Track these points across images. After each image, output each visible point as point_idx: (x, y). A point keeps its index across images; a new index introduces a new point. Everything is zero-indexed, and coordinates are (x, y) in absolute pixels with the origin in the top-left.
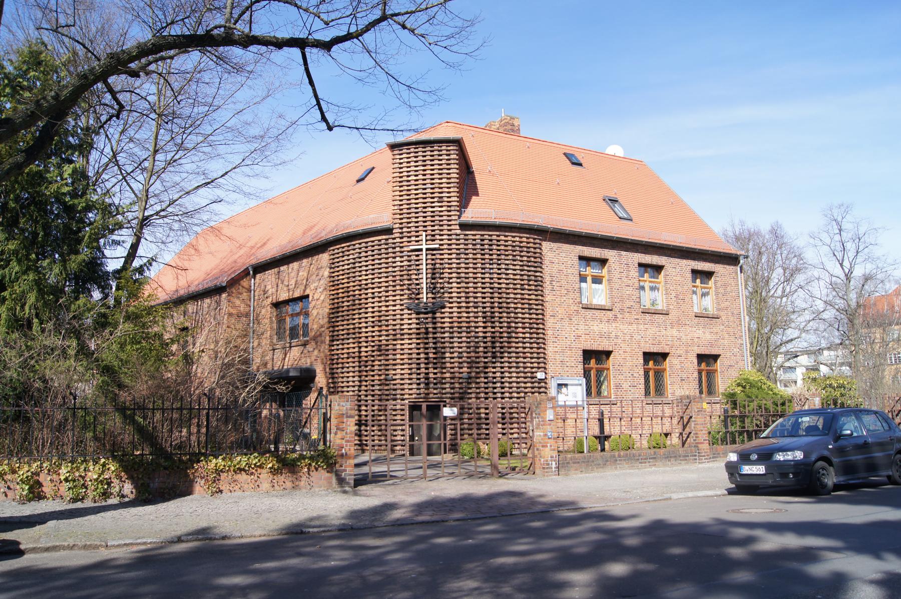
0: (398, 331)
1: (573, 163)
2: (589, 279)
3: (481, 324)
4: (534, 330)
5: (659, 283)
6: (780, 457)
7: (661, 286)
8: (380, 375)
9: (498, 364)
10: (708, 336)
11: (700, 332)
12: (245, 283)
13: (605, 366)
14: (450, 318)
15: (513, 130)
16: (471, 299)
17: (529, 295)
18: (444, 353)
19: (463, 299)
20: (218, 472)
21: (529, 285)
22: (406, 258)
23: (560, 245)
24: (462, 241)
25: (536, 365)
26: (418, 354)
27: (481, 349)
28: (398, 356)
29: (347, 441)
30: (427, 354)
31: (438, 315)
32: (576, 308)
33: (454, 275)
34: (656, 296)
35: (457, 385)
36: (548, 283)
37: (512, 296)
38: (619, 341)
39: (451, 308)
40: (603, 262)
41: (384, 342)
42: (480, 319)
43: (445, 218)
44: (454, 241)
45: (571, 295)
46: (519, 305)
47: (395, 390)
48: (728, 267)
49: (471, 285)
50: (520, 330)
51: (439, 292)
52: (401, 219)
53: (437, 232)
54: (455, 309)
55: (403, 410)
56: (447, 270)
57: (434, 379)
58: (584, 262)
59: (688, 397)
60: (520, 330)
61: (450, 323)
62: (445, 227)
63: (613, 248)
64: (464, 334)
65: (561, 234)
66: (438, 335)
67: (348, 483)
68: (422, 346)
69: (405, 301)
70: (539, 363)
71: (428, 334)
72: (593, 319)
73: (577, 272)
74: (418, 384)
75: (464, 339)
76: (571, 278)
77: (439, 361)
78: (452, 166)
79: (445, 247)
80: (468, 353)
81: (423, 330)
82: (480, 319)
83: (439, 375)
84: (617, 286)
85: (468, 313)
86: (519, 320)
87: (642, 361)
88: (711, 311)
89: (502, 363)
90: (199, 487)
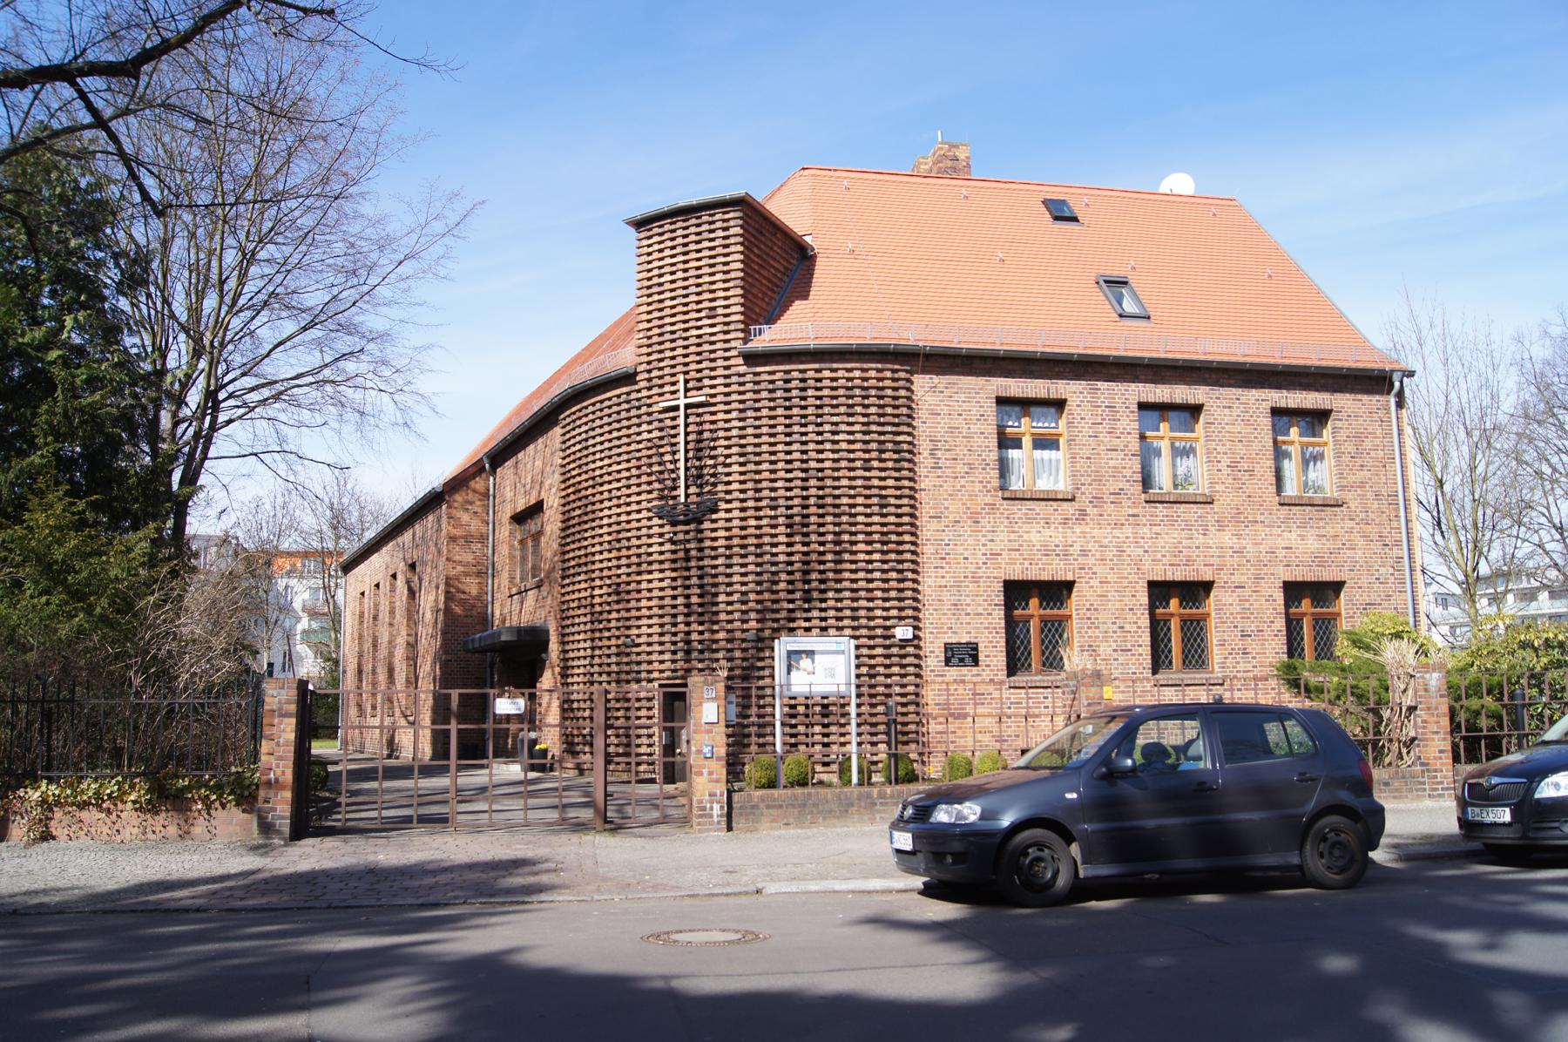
0: (644, 558)
1: (1057, 218)
2: (1027, 441)
3: (782, 539)
5: (1326, 444)
6: (942, 815)
7: (1199, 447)
9: (815, 613)
10: (1312, 544)
11: (1294, 536)
12: (478, 484)
13: (1062, 612)
14: (728, 529)
15: (954, 169)
16: (766, 493)
17: (881, 479)
18: (716, 595)
19: (750, 494)
20: (46, 805)
21: (882, 460)
22: (656, 424)
24: (749, 386)
25: (894, 613)
26: (674, 597)
27: (782, 585)
28: (644, 603)
29: (280, 758)
30: (688, 597)
31: (707, 525)
32: (988, 500)
33: (735, 450)
35: (737, 654)
36: (926, 454)
37: (845, 482)
38: (1091, 561)
39: (728, 511)
40: (1059, 405)
41: (624, 578)
42: (782, 529)
43: (719, 346)
44: (735, 388)
45: (979, 475)
46: (860, 500)
47: (639, 663)
48: (1365, 398)
49: (765, 466)
50: (862, 547)
51: (707, 483)
52: (649, 354)
53: (706, 373)
54: (736, 513)
55: (650, 699)
56: (723, 442)
57: (700, 642)
60: (862, 547)
62: (720, 363)
63: (1077, 376)
64: (751, 559)
67: (279, 832)
68: (679, 582)
69: (655, 503)
70: (901, 609)
72: (1029, 520)
73: (993, 430)
74: (674, 652)
75: (751, 568)
76: (978, 441)
77: (706, 611)
79: (720, 398)
80: (758, 593)
82: (782, 529)
83: (707, 635)
84: (1086, 452)
85: (758, 518)
87: (1145, 600)
88: (1330, 493)
89: (822, 610)
90: (19, 830)
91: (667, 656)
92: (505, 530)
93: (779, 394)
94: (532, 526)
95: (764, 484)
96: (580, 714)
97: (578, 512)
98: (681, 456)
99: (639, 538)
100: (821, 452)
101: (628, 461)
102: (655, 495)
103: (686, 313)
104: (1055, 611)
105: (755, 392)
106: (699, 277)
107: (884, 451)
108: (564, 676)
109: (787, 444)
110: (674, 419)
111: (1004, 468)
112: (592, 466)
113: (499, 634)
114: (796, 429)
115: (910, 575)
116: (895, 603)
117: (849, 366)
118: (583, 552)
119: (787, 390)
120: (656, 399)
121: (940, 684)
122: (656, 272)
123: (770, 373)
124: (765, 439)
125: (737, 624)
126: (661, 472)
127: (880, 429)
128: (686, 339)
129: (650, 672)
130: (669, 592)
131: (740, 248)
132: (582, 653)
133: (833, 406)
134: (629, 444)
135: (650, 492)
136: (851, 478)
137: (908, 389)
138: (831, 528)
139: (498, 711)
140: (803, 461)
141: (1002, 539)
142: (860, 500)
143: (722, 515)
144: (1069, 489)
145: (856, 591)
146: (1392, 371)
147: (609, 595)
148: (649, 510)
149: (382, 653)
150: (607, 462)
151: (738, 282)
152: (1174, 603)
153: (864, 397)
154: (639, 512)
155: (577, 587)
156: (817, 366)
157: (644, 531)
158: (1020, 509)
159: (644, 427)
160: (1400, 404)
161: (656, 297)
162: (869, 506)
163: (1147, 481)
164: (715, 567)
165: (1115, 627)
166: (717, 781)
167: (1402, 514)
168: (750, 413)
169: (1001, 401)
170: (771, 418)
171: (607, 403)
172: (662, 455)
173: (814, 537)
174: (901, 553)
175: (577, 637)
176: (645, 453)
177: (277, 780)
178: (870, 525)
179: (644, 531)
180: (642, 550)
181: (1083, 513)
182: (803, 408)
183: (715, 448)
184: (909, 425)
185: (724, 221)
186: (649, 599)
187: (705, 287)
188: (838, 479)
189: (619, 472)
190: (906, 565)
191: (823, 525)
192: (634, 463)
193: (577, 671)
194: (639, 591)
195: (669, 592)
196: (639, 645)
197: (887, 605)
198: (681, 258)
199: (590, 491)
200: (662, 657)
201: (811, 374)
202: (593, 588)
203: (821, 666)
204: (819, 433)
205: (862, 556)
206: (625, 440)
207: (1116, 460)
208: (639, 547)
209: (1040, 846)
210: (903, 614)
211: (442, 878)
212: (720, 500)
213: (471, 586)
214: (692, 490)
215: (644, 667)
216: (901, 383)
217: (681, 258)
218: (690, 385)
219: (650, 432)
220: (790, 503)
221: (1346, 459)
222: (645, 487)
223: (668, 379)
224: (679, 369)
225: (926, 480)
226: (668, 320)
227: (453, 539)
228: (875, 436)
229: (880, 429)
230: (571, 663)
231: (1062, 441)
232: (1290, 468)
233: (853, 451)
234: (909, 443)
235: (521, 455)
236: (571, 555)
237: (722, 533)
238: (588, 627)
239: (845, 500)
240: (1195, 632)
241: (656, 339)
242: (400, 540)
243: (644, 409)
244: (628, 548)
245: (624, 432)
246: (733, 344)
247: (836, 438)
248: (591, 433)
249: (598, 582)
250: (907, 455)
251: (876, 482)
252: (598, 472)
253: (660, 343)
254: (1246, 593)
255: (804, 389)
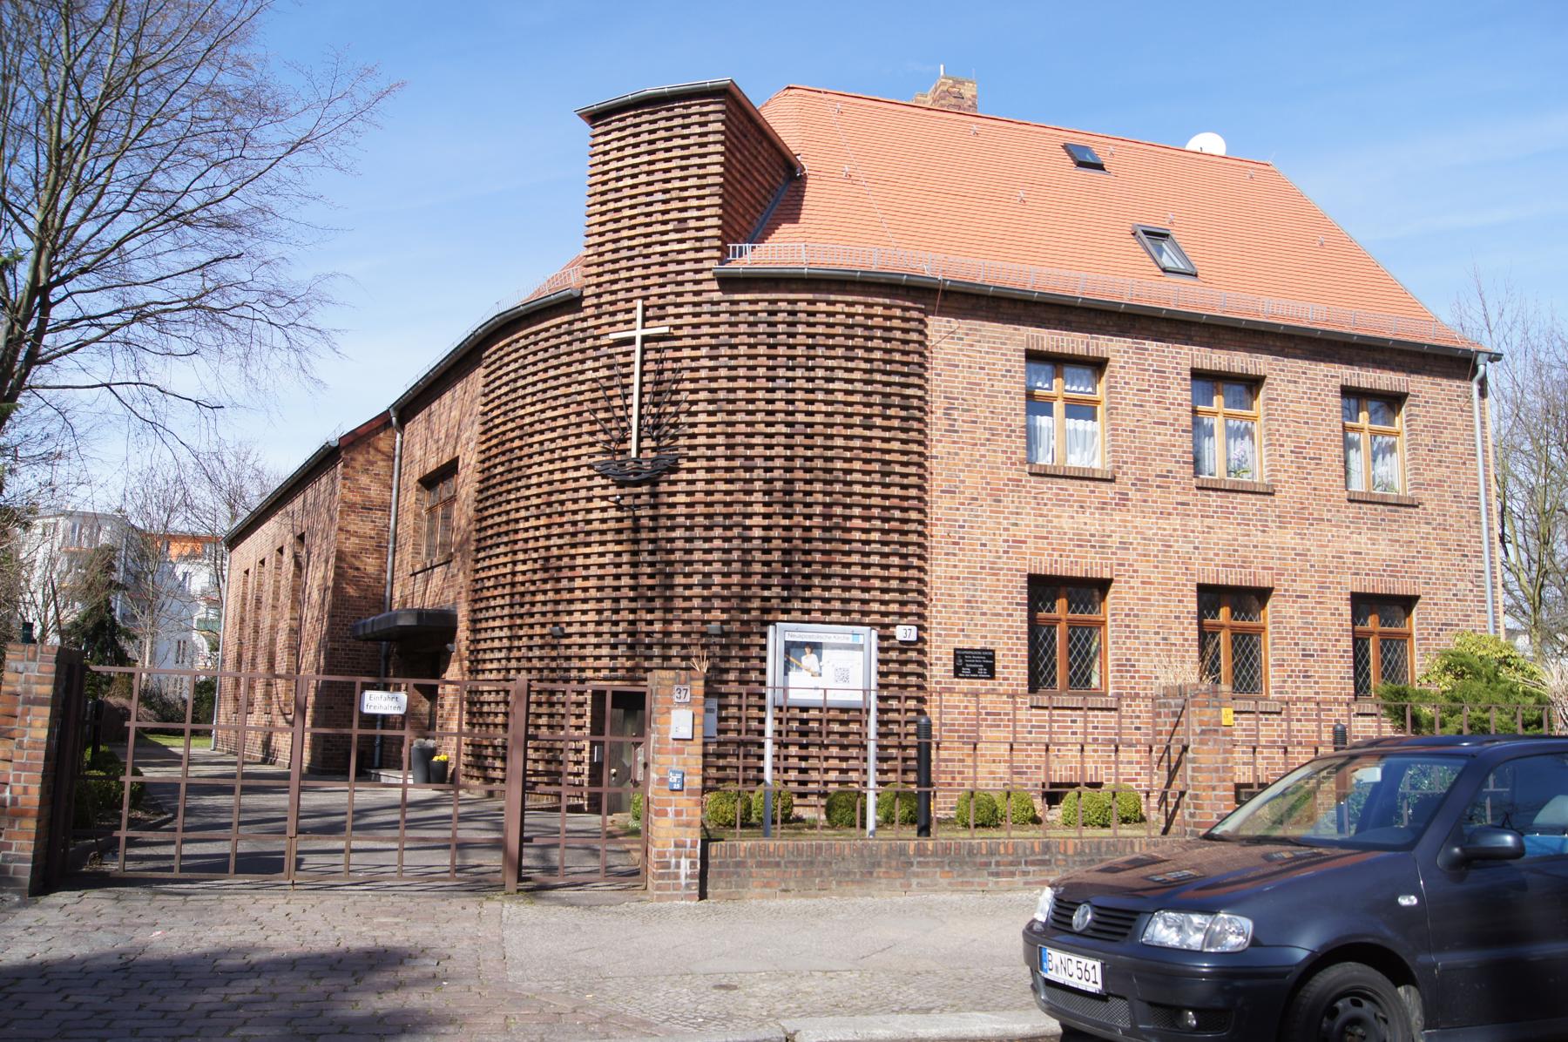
1: (1081, 164)
2: (1059, 407)
4: (895, 524)
6: (1164, 931)
7: (1256, 428)
8: (543, 625)
10: (1384, 550)
11: (1363, 538)
13: (1093, 617)
14: (689, 494)
17: (885, 440)
18: (671, 575)
19: (720, 451)
22: (604, 361)
23: (976, 324)
24: (724, 317)
25: (894, 607)
26: (617, 577)
27: (757, 567)
28: (578, 583)
31: (664, 487)
32: (1013, 474)
33: (703, 395)
34: (1242, 446)
36: (939, 413)
37: (839, 442)
39: (691, 471)
40: (1097, 366)
41: (555, 551)
42: (758, 496)
43: (688, 266)
44: (706, 318)
45: (1002, 443)
46: (857, 465)
47: (568, 658)
48: (1445, 382)
50: (857, 523)
51: (665, 435)
52: (599, 275)
53: (671, 298)
54: (701, 474)
58: (1048, 367)
59: (1180, 690)
60: (857, 523)
61: (688, 505)
62: (689, 287)
63: (1122, 333)
65: (978, 296)
66: (662, 534)
68: (625, 558)
69: (599, 458)
70: (903, 603)
71: (643, 536)
72: (1061, 502)
73: (1019, 390)
75: (717, 543)
78: (711, 148)
80: (725, 575)
81: (628, 523)
84: (1130, 423)
86: (856, 499)
87: (1194, 607)
88: (1401, 487)
89: (805, 600)
91: (605, 651)
92: (410, 498)
93: (761, 328)
94: (443, 491)
95: (739, 439)
96: (490, 719)
97: (500, 469)
98: (635, 400)
99: (575, 501)
100: (811, 402)
101: (567, 406)
102: (598, 448)
103: (647, 225)
104: (1086, 616)
105: (732, 324)
106: (667, 181)
107: (889, 406)
108: (473, 671)
109: (769, 390)
110: (627, 354)
111: (1031, 436)
112: (522, 412)
113: (396, 616)
114: (781, 372)
115: (915, 562)
116: (896, 596)
117: (850, 298)
118: (504, 518)
119: (771, 324)
120: (605, 329)
121: (950, 703)
122: (613, 175)
123: (751, 302)
124: (742, 383)
125: (697, 614)
126: (608, 420)
127: (885, 378)
128: (647, 256)
129: (582, 670)
130: (611, 570)
131: (720, 148)
132: (497, 644)
133: (828, 347)
134: (568, 385)
135: (592, 445)
136: (847, 437)
137: (921, 332)
138: (820, 498)
139: (366, 710)
140: (788, 413)
141: (1028, 523)
142: (857, 465)
143: (684, 476)
144: (1108, 467)
145: (848, 577)
146: (1478, 352)
147: (535, 571)
148: (590, 467)
149: (263, 641)
150: (539, 407)
151: (715, 189)
152: (1224, 612)
153: (867, 338)
154: (577, 469)
155: (495, 561)
156: (810, 296)
157: (583, 493)
158: (1049, 488)
159: (589, 364)
160: (1483, 394)
161: (612, 205)
162: (868, 473)
163: (1197, 463)
164: (672, 540)
165: (1158, 639)
166: (688, 825)
167: (1484, 520)
168: (724, 351)
169: (1033, 356)
170: (750, 357)
171: (544, 335)
172: (610, 398)
173: (798, 509)
174: (905, 533)
175: (491, 624)
176: (588, 395)
177: (14, 801)
178: (869, 496)
179: (583, 493)
180: (579, 517)
181: (1124, 497)
182: (790, 347)
183: (677, 392)
184: (920, 376)
185: (702, 114)
186: (586, 578)
187: (674, 194)
188: (831, 437)
189: (554, 419)
190: (911, 549)
191: (809, 493)
192: (574, 408)
193: (489, 666)
194: (572, 568)
195: (611, 570)
196: (569, 635)
197: (887, 597)
198: (646, 158)
199: (517, 443)
200: (597, 652)
201: (802, 306)
202: (514, 563)
203: (831, 667)
204: (810, 380)
205: (857, 535)
206: (564, 380)
207: (1164, 436)
208: (575, 512)
209: (1358, 995)
210: (906, 610)
211: (240, 991)
212: (682, 457)
213: (370, 564)
214: (647, 443)
215: (576, 663)
216: (913, 325)
217: (646, 158)
218: (650, 313)
219: (595, 370)
220: (770, 464)
221: (1422, 452)
222: (586, 438)
223: (622, 305)
224: (637, 293)
225: (938, 447)
226: (625, 233)
227: (351, 507)
228: (879, 387)
229: (885, 378)
230: (483, 645)
231: (1100, 410)
232: (1357, 460)
233: (851, 404)
234: (920, 398)
235: (435, 406)
236: (490, 522)
237: (682, 498)
238: (506, 611)
239: (839, 464)
240: (1247, 646)
241: (608, 256)
242: (289, 508)
243: (590, 342)
244: (562, 514)
245: (564, 370)
246: (706, 264)
247: (831, 386)
248: (522, 372)
249: (521, 556)
250: (917, 414)
251: (878, 444)
252: (528, 420)
253: (614, 262)
254: (1309, 604)
255: (793, 324)
